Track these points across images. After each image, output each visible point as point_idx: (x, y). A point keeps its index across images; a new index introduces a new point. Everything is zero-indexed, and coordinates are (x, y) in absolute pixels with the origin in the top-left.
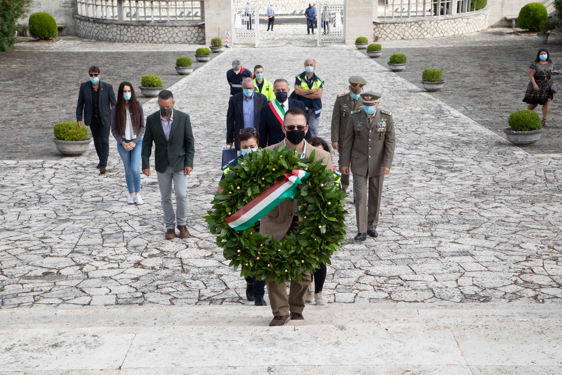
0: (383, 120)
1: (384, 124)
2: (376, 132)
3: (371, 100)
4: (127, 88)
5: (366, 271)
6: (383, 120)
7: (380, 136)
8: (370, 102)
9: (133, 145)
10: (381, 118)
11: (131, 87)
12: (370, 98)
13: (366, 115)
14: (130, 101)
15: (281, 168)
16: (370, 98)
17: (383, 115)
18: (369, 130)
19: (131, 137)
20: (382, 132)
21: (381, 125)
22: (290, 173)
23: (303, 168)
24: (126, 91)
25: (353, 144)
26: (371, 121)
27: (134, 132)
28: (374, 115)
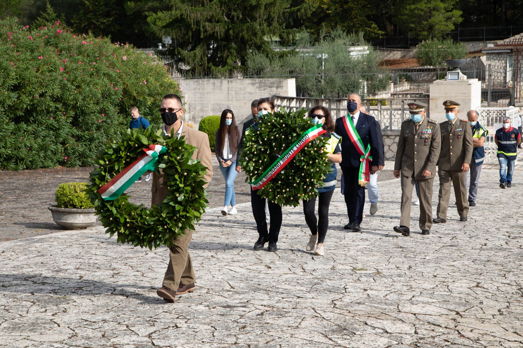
0: (429, 128)
1: (430, 131)
2: (421, 138)
3: (416, 108)
4: (229, 115)
5: (498, 287)
6: (429, 128)
7: (425, 142)
8: (415, 111)
9: (229, 163)
10: (427, 126)
11: (233, 115)
12: (415, 107)
13: (414, 123)
14: (230, 126)
15: (142, 145)
16: (415, 107)
17: (430, 124)
18: (415, 135)
19: (228, 156)
20: (426, 139)
21: (427, 132)
22: (148, 148)
23: (161, 144)
24: (228, 118)
25: (404, 150)
26: (418, 128)
27: (231, 152)
28: (420, 123)
